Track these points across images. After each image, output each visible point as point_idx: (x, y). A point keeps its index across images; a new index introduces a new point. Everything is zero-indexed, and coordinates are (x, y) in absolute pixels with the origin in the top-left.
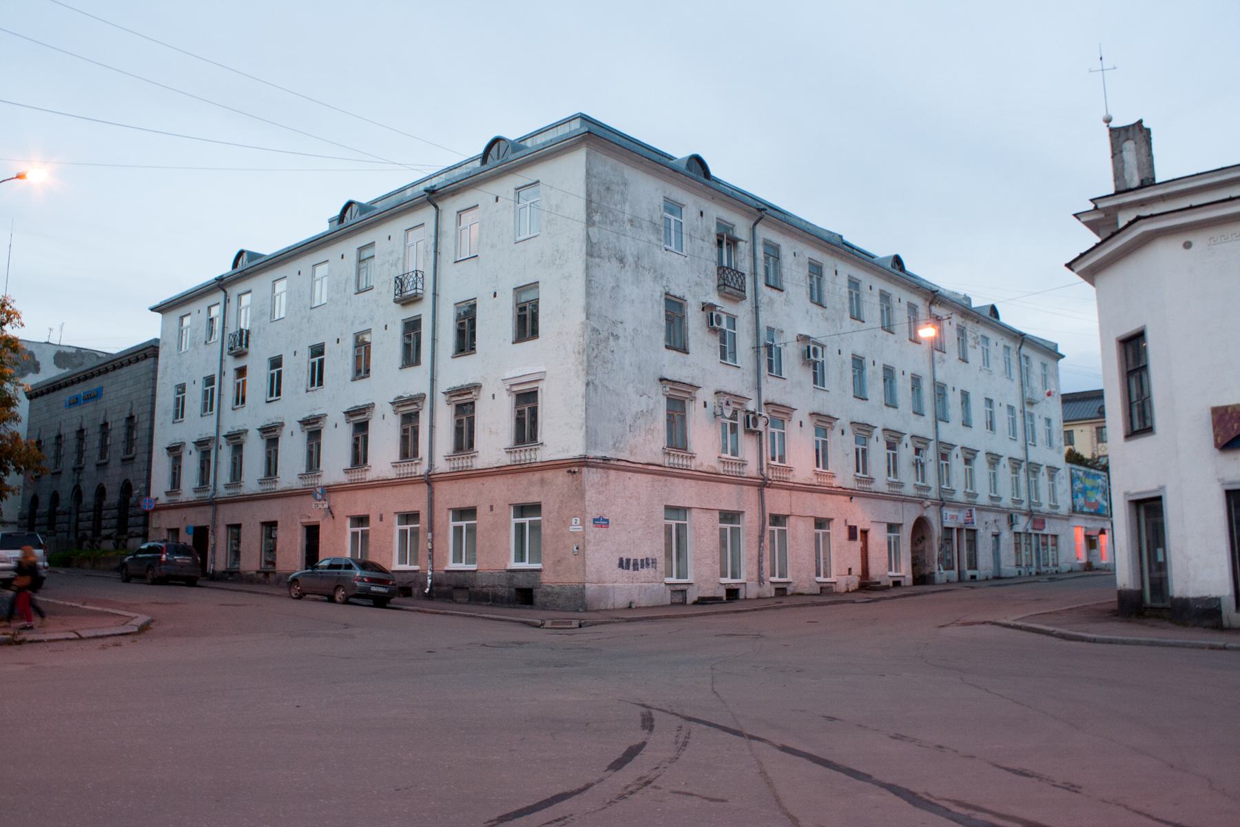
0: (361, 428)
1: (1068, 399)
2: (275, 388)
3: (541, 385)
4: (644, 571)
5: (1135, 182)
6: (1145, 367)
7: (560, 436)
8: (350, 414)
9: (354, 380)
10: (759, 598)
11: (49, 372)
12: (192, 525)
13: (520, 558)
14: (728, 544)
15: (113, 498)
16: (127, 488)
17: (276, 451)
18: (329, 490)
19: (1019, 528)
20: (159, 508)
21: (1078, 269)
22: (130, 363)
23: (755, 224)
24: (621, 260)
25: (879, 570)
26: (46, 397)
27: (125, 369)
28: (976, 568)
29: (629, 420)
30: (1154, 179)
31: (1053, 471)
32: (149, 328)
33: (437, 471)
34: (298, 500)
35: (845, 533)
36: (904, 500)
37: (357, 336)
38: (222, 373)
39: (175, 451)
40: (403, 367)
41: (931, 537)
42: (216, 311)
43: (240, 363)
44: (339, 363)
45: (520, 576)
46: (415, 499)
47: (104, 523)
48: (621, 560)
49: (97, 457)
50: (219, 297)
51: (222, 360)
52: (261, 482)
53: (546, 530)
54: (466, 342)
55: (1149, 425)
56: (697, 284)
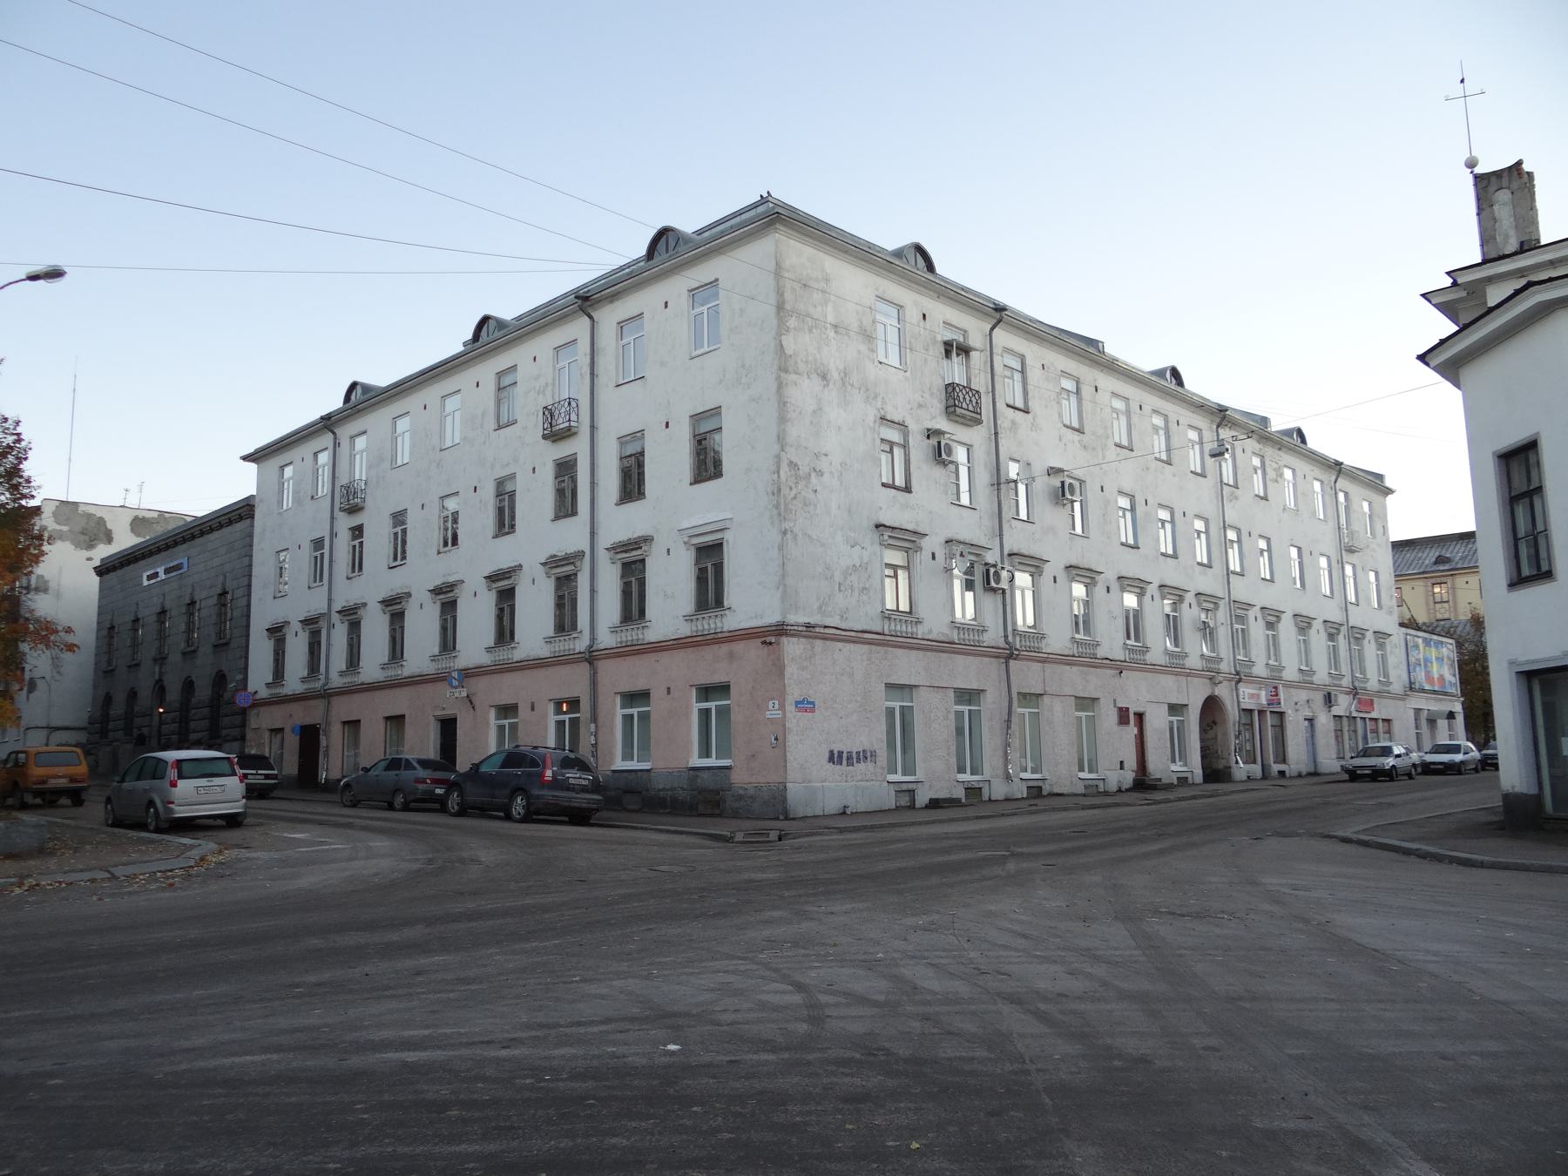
0: (506, 597)
1: (1399, 546)
2: (400, 551)
3: (728, 536)
4: (861, 766)
5: (1512, 246)
6: (1539, 489)
7: (748, 603)
8: (492, 578)
9: (496, 536)
10: (1007, 800)
11: (125, 540)
12: (299, 723)
13: (705, 752)
14: (966, 733)
15: (203, 692)
16: (220, 679)
17: (402, 628)
18: (468, 674)
19: (1337, 711)
20: (259, 704)
21: (1433, 364)
22: (221, 526)
23: (992, 329)
24: (824, 377)
25: (1161, 765)
26: (119, 572)
27: (216, 535)
28: (1284, 761)
29: (838, 577)
30: (1538, 241)
31: (1381, 636)
32: (242, 483)
33: (601, 646)
34: (429, 687)
35: (1113, 717)
36: (1191, 674)
37: (500, 483)
38: (333, 535)
39: (277, 632)
40: (557, 518)
41: (1224, 721)
42: (324, 458)
43: (355, 521)
44: (478, 519)
45: (705, 775)
46: (574, 681)
47: (192, 725)
48: (832, 752)
49: (183, 645)
50: (326, 439)
51: (332, 518)
52: (384, 667)
53: (737, 717)
54: (632, 484)
55: (1544, 568)
56: (920, 406)
